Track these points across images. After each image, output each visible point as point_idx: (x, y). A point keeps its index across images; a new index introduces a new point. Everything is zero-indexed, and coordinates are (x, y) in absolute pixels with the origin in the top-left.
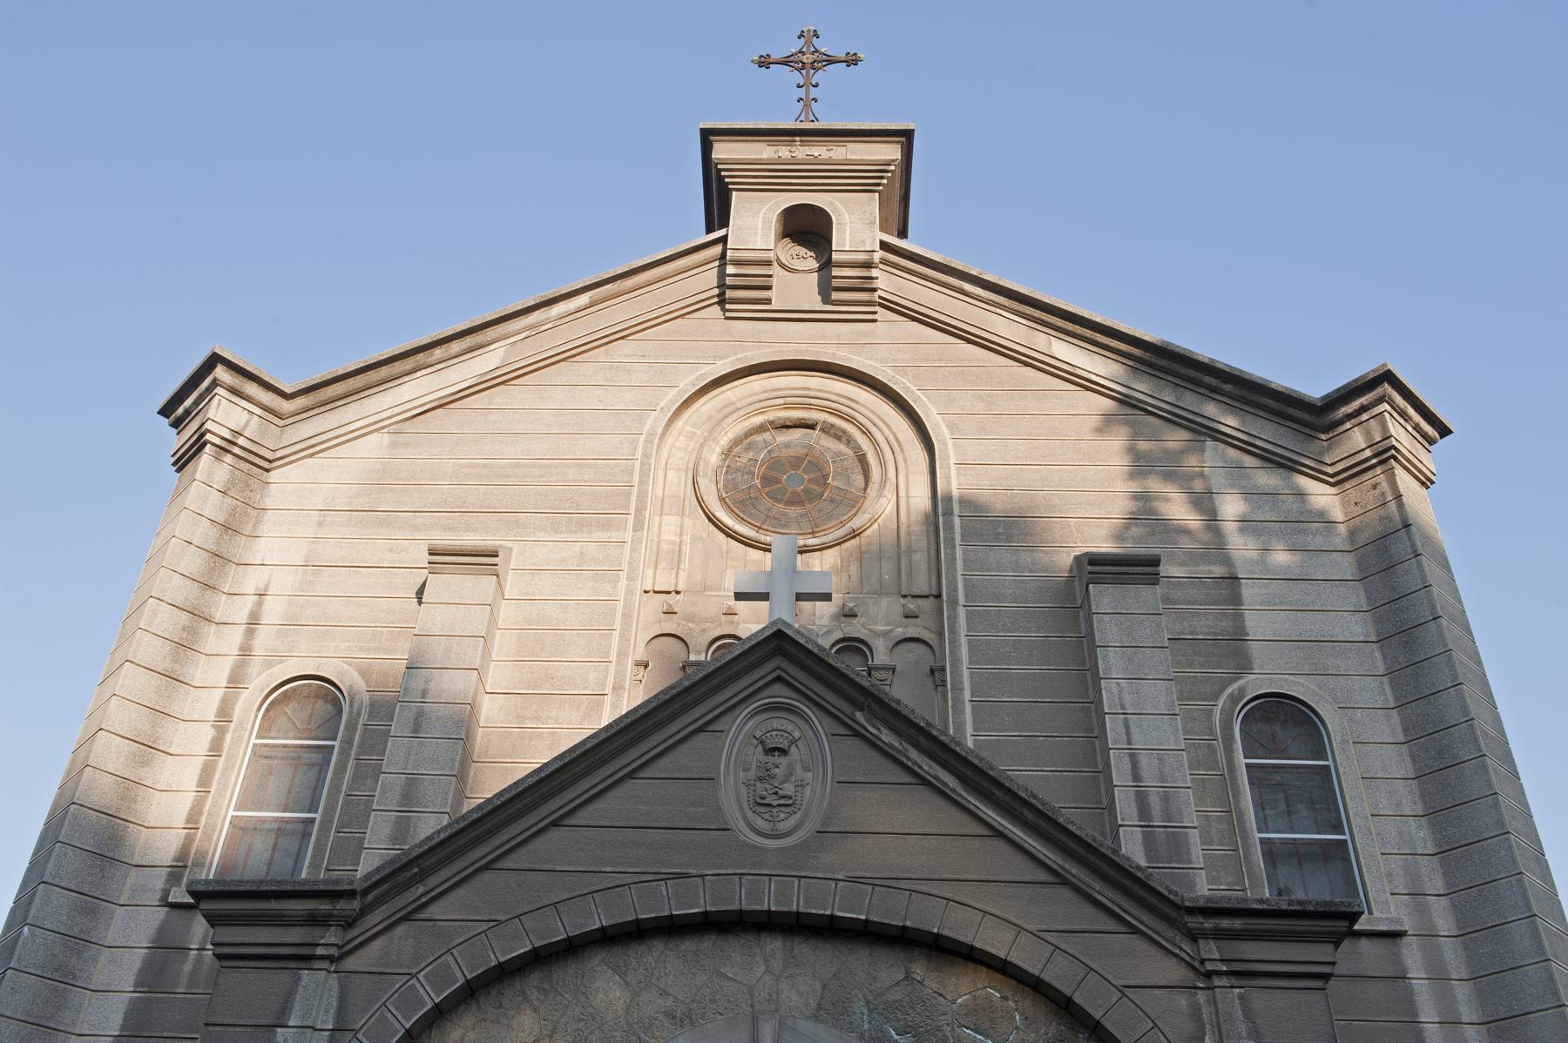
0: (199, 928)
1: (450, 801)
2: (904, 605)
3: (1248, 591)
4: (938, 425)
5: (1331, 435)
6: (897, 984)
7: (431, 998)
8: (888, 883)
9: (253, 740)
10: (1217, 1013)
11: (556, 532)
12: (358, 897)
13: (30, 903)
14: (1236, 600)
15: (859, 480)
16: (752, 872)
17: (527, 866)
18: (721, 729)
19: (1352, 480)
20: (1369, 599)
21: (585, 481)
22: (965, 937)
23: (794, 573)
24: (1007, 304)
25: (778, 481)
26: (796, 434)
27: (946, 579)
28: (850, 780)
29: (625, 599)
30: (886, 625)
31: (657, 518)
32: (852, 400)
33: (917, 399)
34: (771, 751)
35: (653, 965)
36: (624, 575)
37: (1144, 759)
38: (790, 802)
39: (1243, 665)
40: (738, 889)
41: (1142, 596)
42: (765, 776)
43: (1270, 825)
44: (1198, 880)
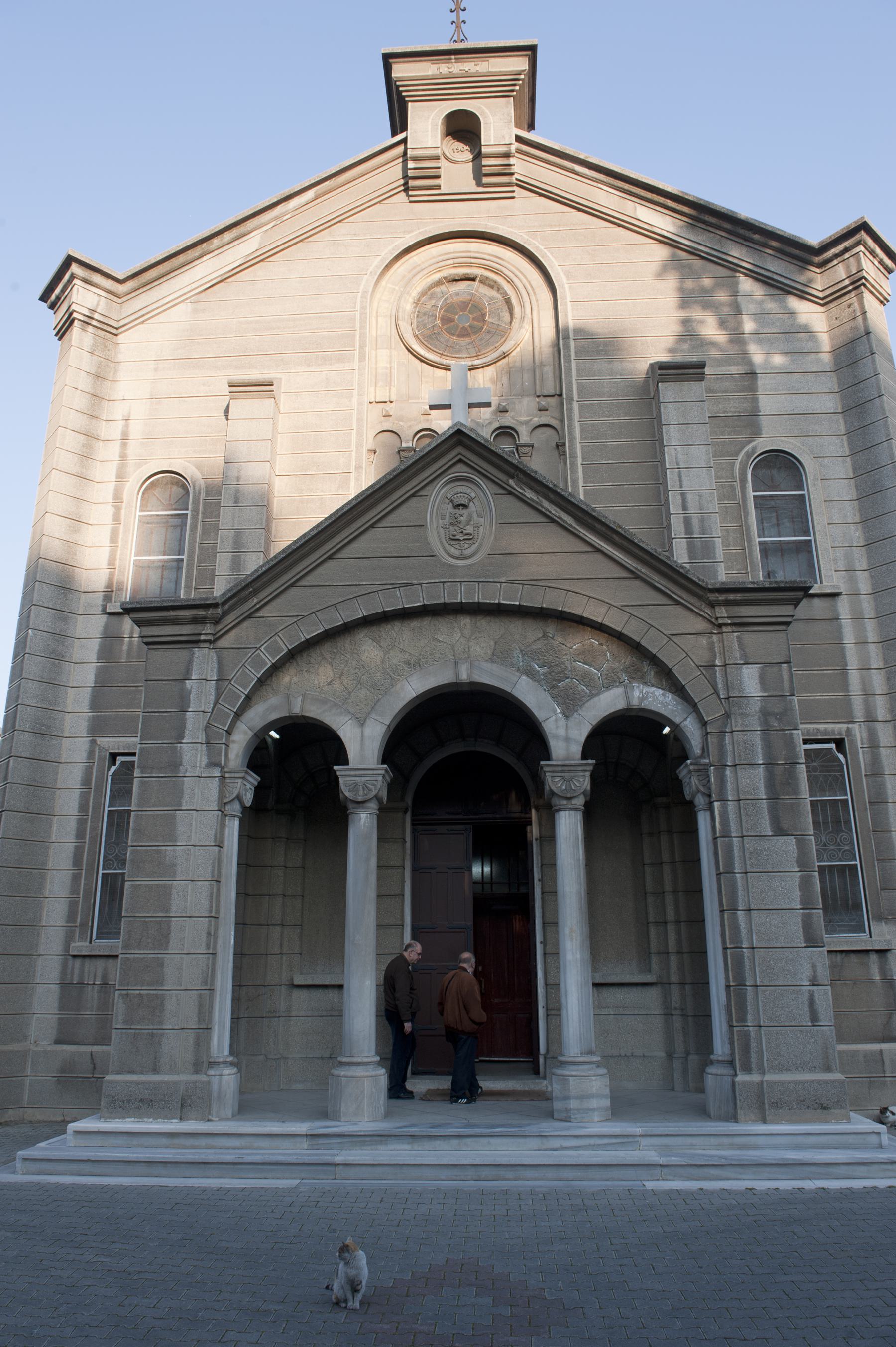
0: (127, 624)
1: (263, 545)
2: (538, 403)
3: (761, 382)
5: (823, 270)
6: (538, 640)
8: (533, 583)
9: (138, 513)
10: (724, 647)
12: (220, 606)
13: (29, 617)
14: (753, 388)
15: (506, 316)
19: (837, 301)
20: (839, 384)
22: (577, 611)
23: (467, 390)
24: (605, 180)
25: (452, 320)
26: (463, 285)
28: (507, 522)
29: (358, 409)
30: (527, 416)
31: (374, 352)
32: (500, 258)
34: (457, 506)
36: (355, 393)
37: (690, 496)
38: (471, 537)
39: (756, 431)
41: (693, 389)
42: (455, 522)
43: (766, 533)
44: (719, 569)
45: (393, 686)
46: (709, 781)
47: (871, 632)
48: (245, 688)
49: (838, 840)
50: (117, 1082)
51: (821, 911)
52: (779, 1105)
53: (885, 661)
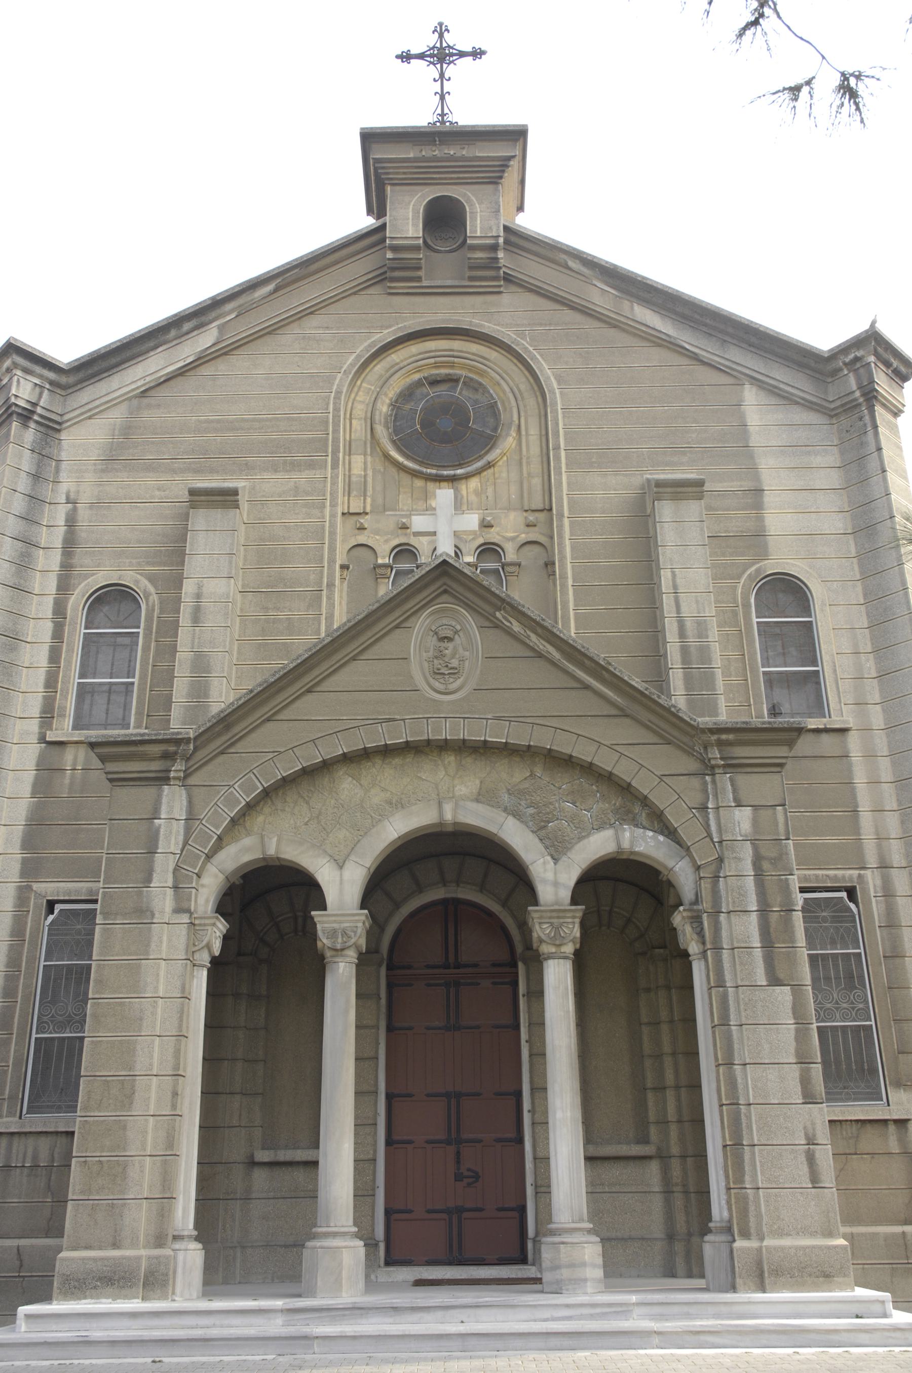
1: (226, 669)
4: (549, 378)
6: (525, 779)
7: (243, 799)
11: (276, 471)
14: (758, 505)
16: (435, 716)
17: (294, 718)
18: (409, 626)
20: (849, 502)
21: (293, 431)
27: (556, 498)
28: (493, 655)
33: (533, 358)
34: (443, 639)
35: (376, 773)
38: (456, 671)
39: (762, 552)
40: (426, 727)
41: (693, 509)
42: (440, 655)
43: (771, 661)
45: (373, 826)
46: (702, 929)
47: (885, 770)
48: (217, 828)
49: (852, 998)
50: (73, 1259)
51: (819, 1066)
52: (780, 1273)
53: (899, 802)
